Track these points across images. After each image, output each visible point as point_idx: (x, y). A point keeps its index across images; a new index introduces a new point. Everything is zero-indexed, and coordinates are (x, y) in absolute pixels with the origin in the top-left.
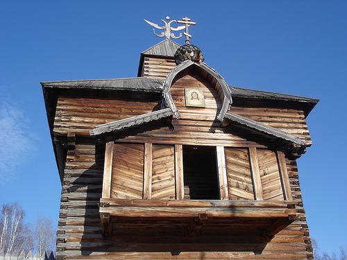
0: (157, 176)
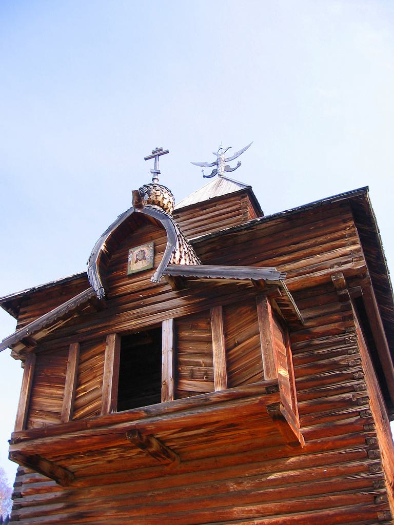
0: (83, 387)
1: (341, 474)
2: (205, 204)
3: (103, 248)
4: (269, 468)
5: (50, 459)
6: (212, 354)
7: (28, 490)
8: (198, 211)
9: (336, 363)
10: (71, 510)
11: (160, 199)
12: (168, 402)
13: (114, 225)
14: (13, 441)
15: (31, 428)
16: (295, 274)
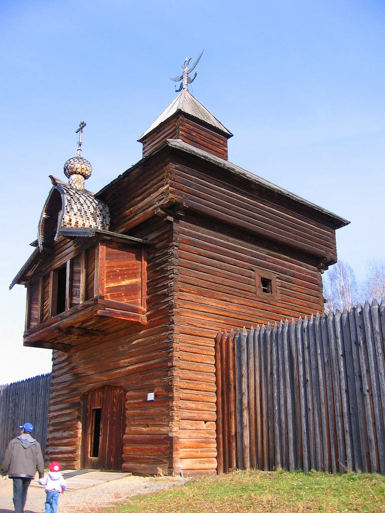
1: (159, 340)
2: (158, 129)
3: (44, 216)
4: (133, 338)
5: (50, 340)
6: (80, 280)
7: (57, 356)
8: (155, 135)
9: (162, 269)
10: (70, 365)
11: (74, 170)
12: (68, 309)
13: (47, 199)
14: (25, 336)
15: (32, 327)
16: (141, 210)
